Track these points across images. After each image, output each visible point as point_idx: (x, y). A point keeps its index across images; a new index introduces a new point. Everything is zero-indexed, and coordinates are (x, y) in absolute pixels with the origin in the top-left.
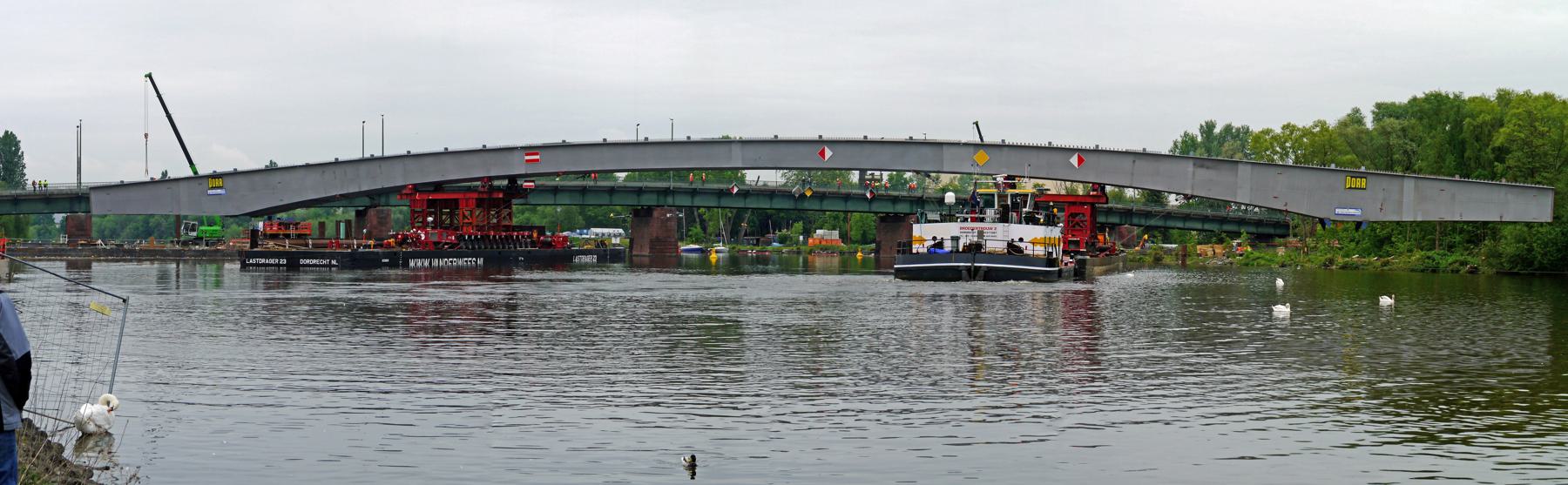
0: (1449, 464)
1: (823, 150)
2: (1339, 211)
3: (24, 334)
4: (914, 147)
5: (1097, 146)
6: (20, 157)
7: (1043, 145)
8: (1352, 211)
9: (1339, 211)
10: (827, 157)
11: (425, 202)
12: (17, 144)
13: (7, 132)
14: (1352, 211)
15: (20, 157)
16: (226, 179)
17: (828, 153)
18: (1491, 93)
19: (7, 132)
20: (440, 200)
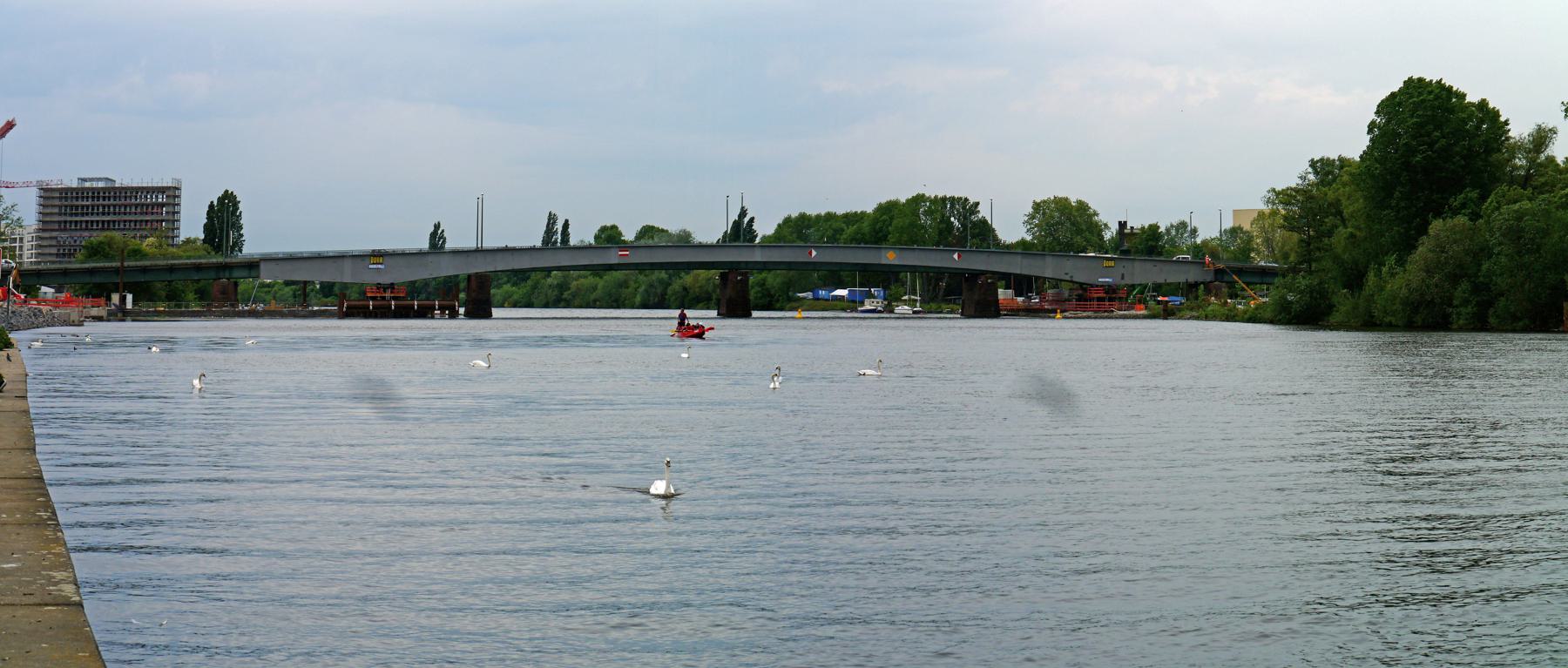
0: (826, 211)
1: (811, 252)
2: (1100, 280)
3: (997, 294)
4: (591, 250)
5: (437, 237)
6: (238, 217)
7: (586, 243)
8: (1107, 280)
9: (1100, 280)
10: (813, 255)
11: (21, 386)
12: (236, 204)
13: (227, 191)
14: (1107, 280)
15: (238, 217)
16: (386, 258)
17: (814, 253)
18: (1473, 98)
19: (227, 191)
20: (633, 307)
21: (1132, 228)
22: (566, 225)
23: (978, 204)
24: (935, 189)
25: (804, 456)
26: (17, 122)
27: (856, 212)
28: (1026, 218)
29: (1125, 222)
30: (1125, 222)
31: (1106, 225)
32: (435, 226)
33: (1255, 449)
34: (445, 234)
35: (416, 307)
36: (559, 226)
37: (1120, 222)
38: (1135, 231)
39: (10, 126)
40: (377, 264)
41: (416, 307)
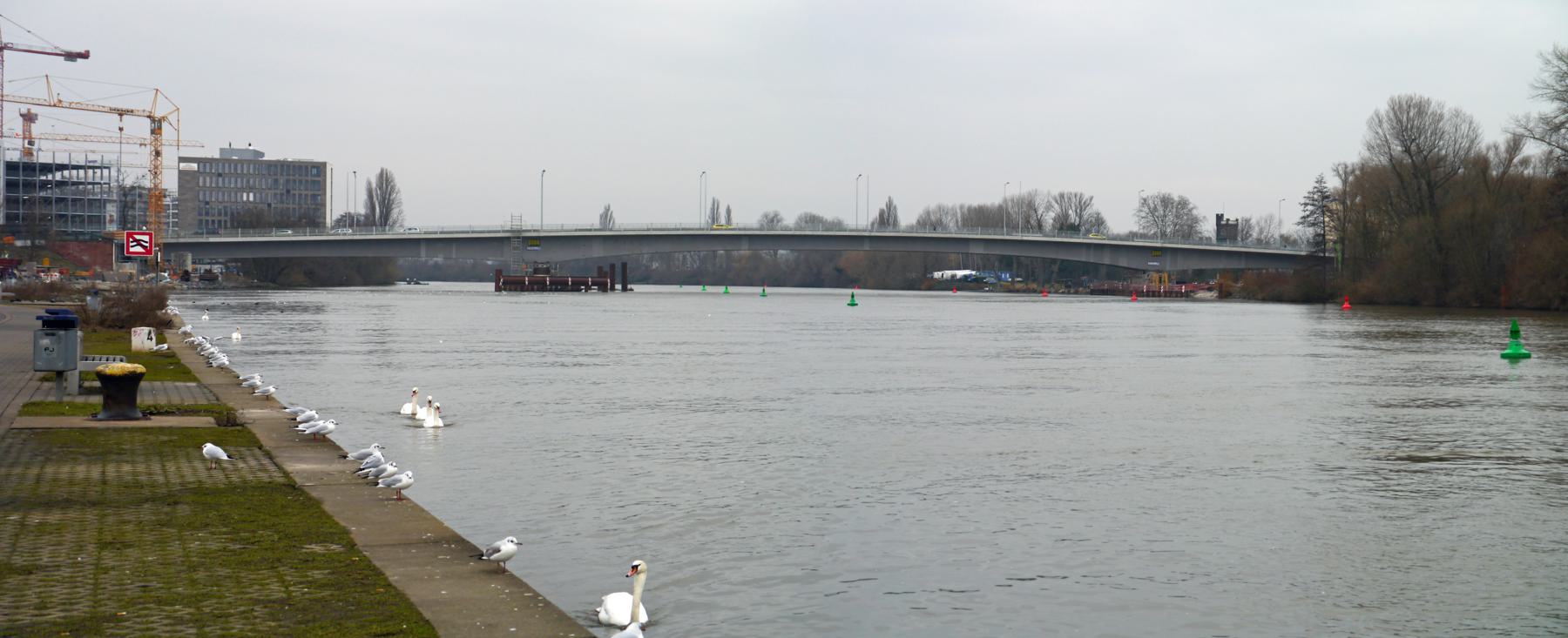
5: (606, 216)
21: (1228, 220)
22: (729, 212)
23: (1091, 198)
24: (990, 196)
25: (1416, 426)
26: (91, 54)
27: (822, 218)
28: (1134, 212)
29: (1222, 215)
30: (1222, 215)
31: (1204, 217)
32: (605, 208)
33: (423, 349)
34: (614, 215)
35: (570, 283)
36: (723, 211)
37: (1217, 215)
38: (1230, 222)
39: (85, 55)
40: (534, 246)
41: (570, 283)
